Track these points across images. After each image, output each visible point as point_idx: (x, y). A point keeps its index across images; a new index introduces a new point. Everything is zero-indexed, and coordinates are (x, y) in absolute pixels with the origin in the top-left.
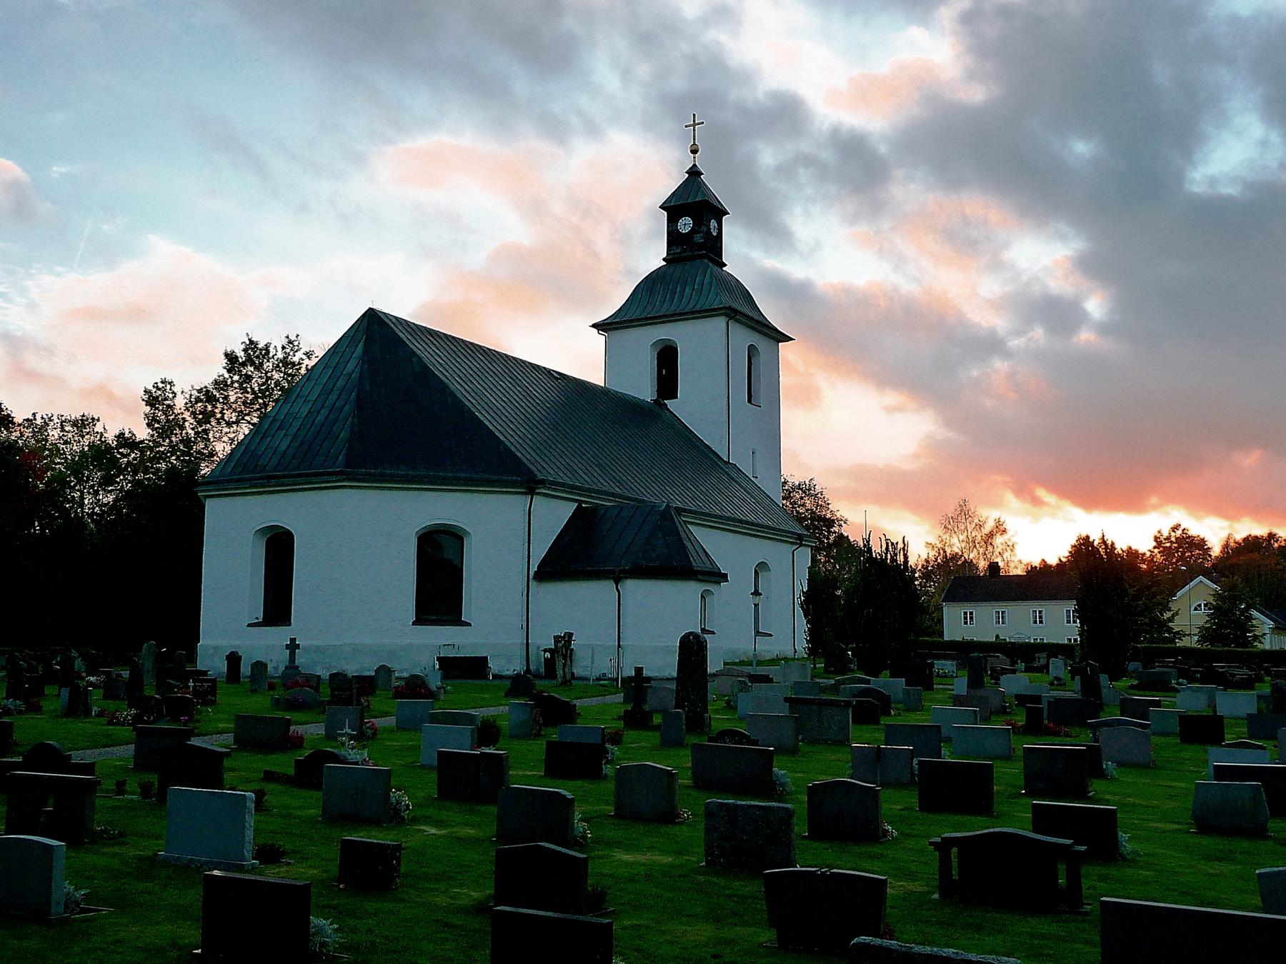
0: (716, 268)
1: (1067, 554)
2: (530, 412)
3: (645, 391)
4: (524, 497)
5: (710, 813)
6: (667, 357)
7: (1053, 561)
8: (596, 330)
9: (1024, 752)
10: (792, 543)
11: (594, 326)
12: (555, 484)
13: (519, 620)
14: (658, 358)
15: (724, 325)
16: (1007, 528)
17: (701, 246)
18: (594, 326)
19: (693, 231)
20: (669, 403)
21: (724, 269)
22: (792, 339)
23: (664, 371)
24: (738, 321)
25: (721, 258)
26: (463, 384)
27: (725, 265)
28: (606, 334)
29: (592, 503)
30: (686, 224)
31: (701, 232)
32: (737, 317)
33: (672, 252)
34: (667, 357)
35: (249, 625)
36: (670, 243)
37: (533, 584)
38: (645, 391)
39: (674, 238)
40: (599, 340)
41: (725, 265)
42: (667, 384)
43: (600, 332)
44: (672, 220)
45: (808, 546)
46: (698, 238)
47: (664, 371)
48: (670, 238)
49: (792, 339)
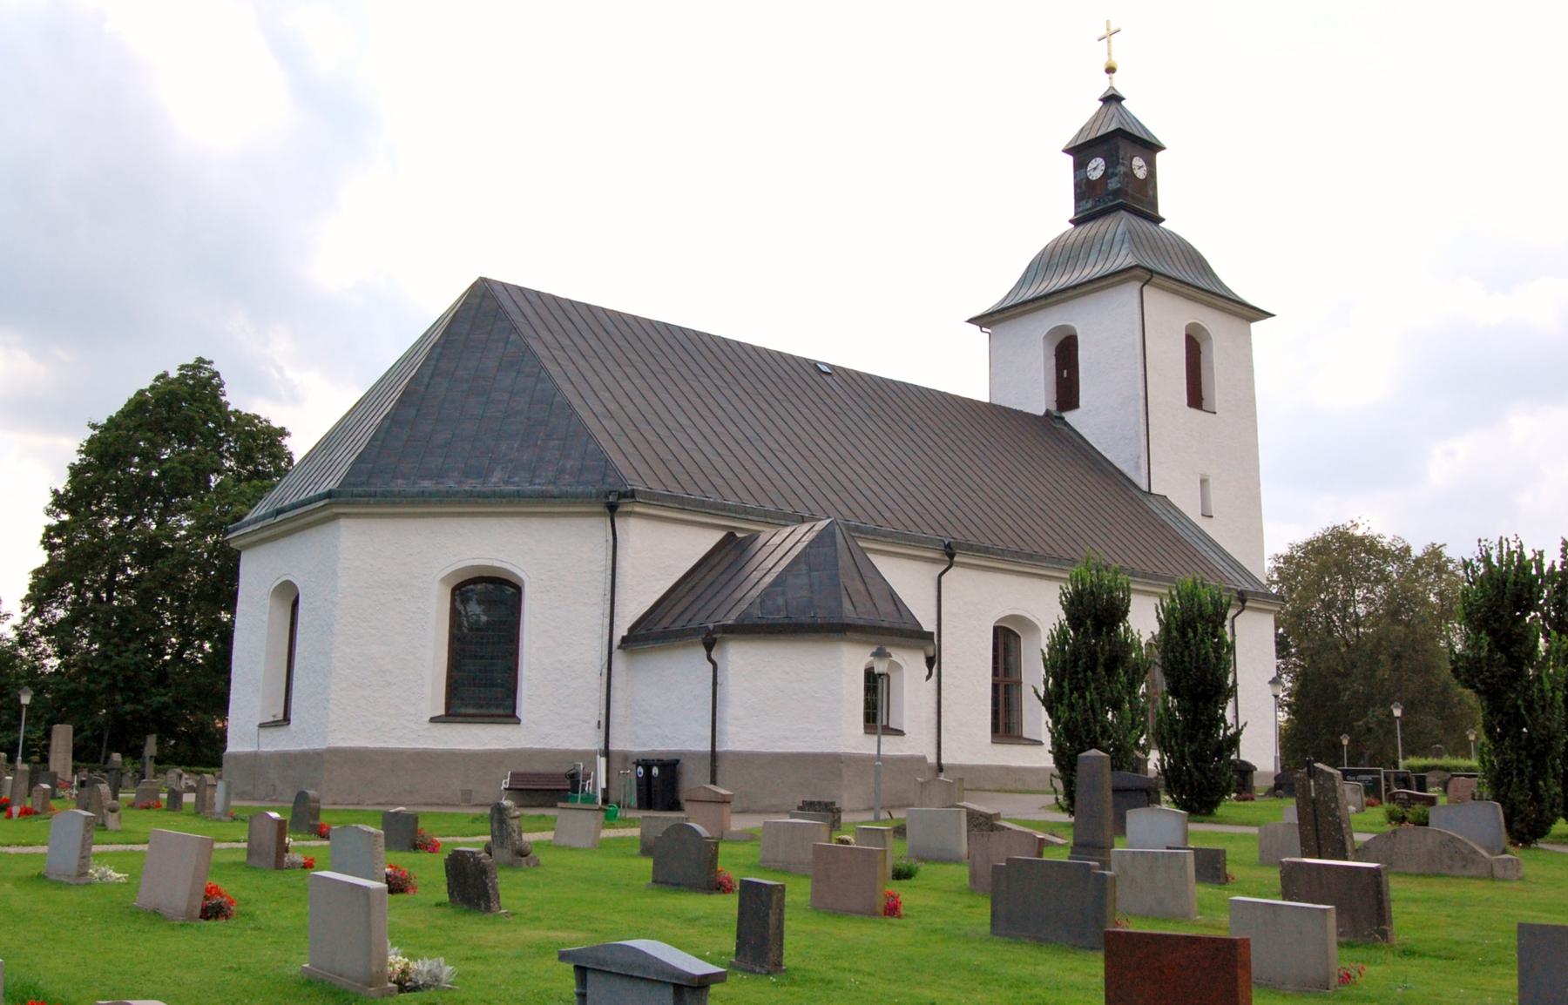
0: (1146, 225)
1: (1470, 552)
2: (1150, 556)
3: (1036, 398)
5: (581, 802)
6: (1066, 352)
8: (978, 328)
9: (993, 872)
11: (971, 321)
15: (1136, 294)
16: (1430, 544)
18: (971, 321)
21: (1161, 225)
22: (1273, 315)
23: (1065, 372)
24: (1157, 286)
25: (1157, 213)
26: (1134, 541)
27: (1162, 220)
28: (989, 331)
30: (1096, 168)
31: (1116, 175)
33: (1081, 209)
34: (1066, 352)
36: (1079, 197)
38: (1036, 398)
39: (1084, 190)
40: (979, 339)
42: (1067, 392)
43: (984, 329)
44: (1080, 166)
46: (1113, 184)
47: (1065, 372)
48: (1078, 191)
49: (1273, 315)
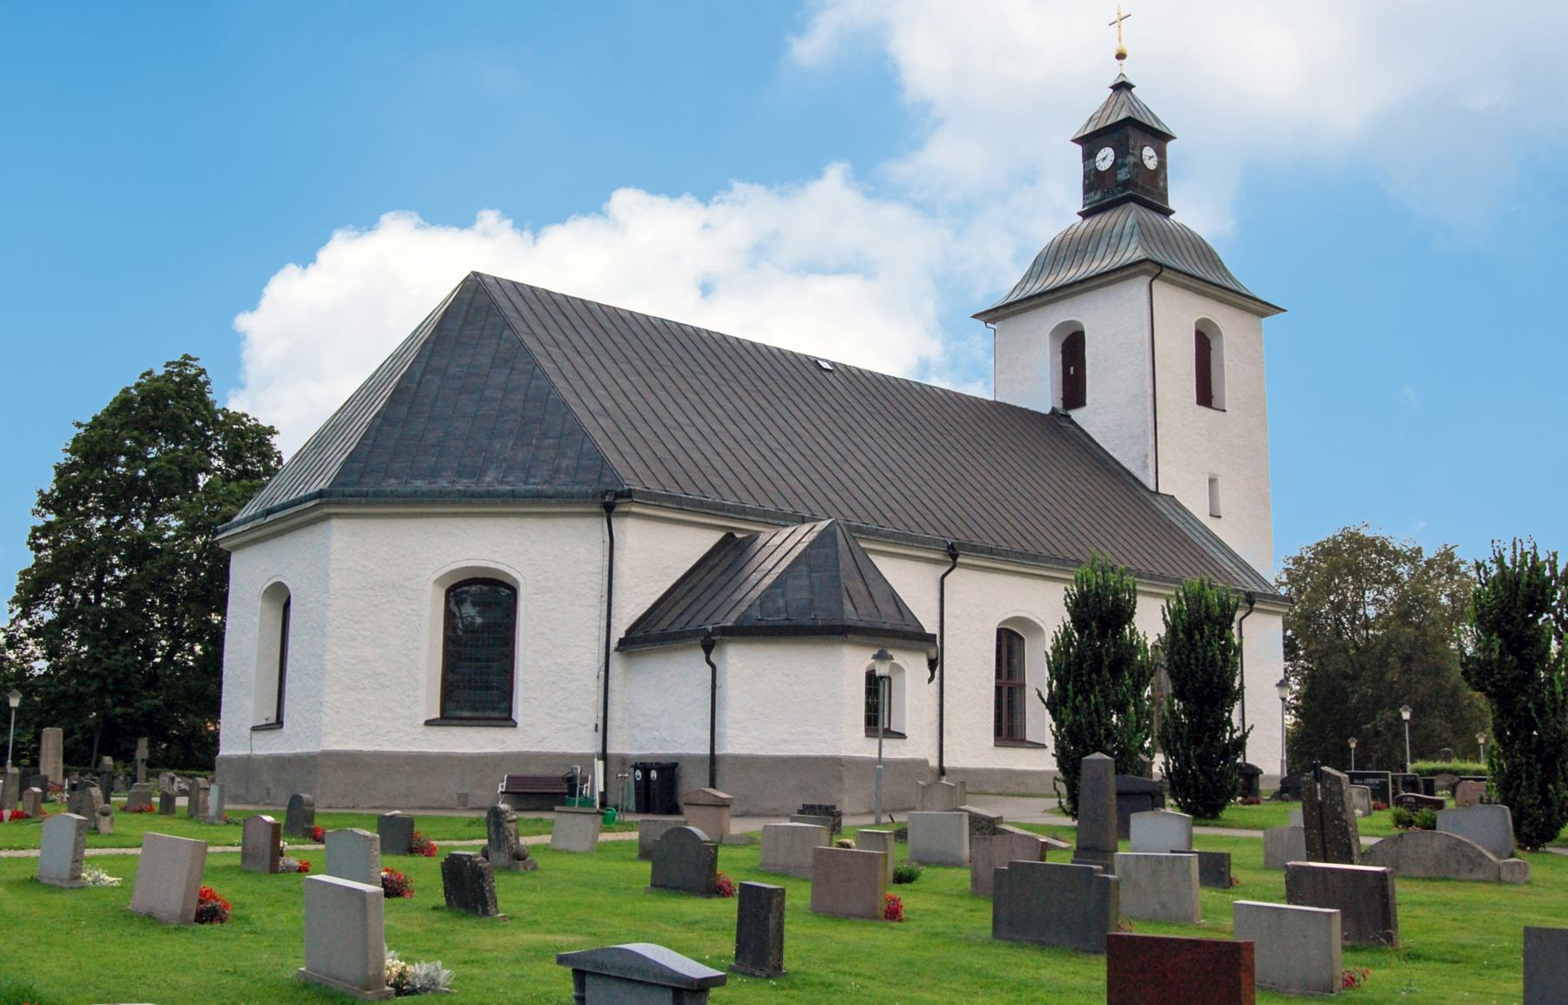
3: (1042, 396)
4: (600, 519)
6: (1073, 348)
7: (291, 270)
10: (936, 562)
12: (650, 498)
13: (593, 715)
14: (1063, 352)
15: (1145, 289)
17: (1126, 184)
19: (1115, 166)
20: (1077, 415)
24: (1167, 280)
27: (1172, 212)
29: (747, 530)
30: (1105, 158)
32: (1164, 274)
34: (1073, 348)
35: (255, 729)
36: (1088, 189)
37: (617, 663)
38: (1042, 396)
39: (1094, 181)
41: (1172, 212)
44: (1089, 156)
45: (1278, 613)
46: (1123, 175)
47: (1072, 369)
